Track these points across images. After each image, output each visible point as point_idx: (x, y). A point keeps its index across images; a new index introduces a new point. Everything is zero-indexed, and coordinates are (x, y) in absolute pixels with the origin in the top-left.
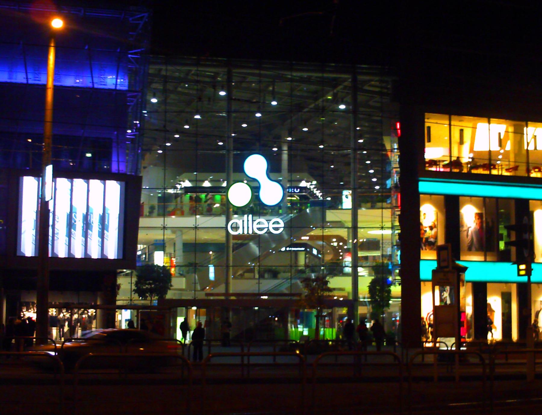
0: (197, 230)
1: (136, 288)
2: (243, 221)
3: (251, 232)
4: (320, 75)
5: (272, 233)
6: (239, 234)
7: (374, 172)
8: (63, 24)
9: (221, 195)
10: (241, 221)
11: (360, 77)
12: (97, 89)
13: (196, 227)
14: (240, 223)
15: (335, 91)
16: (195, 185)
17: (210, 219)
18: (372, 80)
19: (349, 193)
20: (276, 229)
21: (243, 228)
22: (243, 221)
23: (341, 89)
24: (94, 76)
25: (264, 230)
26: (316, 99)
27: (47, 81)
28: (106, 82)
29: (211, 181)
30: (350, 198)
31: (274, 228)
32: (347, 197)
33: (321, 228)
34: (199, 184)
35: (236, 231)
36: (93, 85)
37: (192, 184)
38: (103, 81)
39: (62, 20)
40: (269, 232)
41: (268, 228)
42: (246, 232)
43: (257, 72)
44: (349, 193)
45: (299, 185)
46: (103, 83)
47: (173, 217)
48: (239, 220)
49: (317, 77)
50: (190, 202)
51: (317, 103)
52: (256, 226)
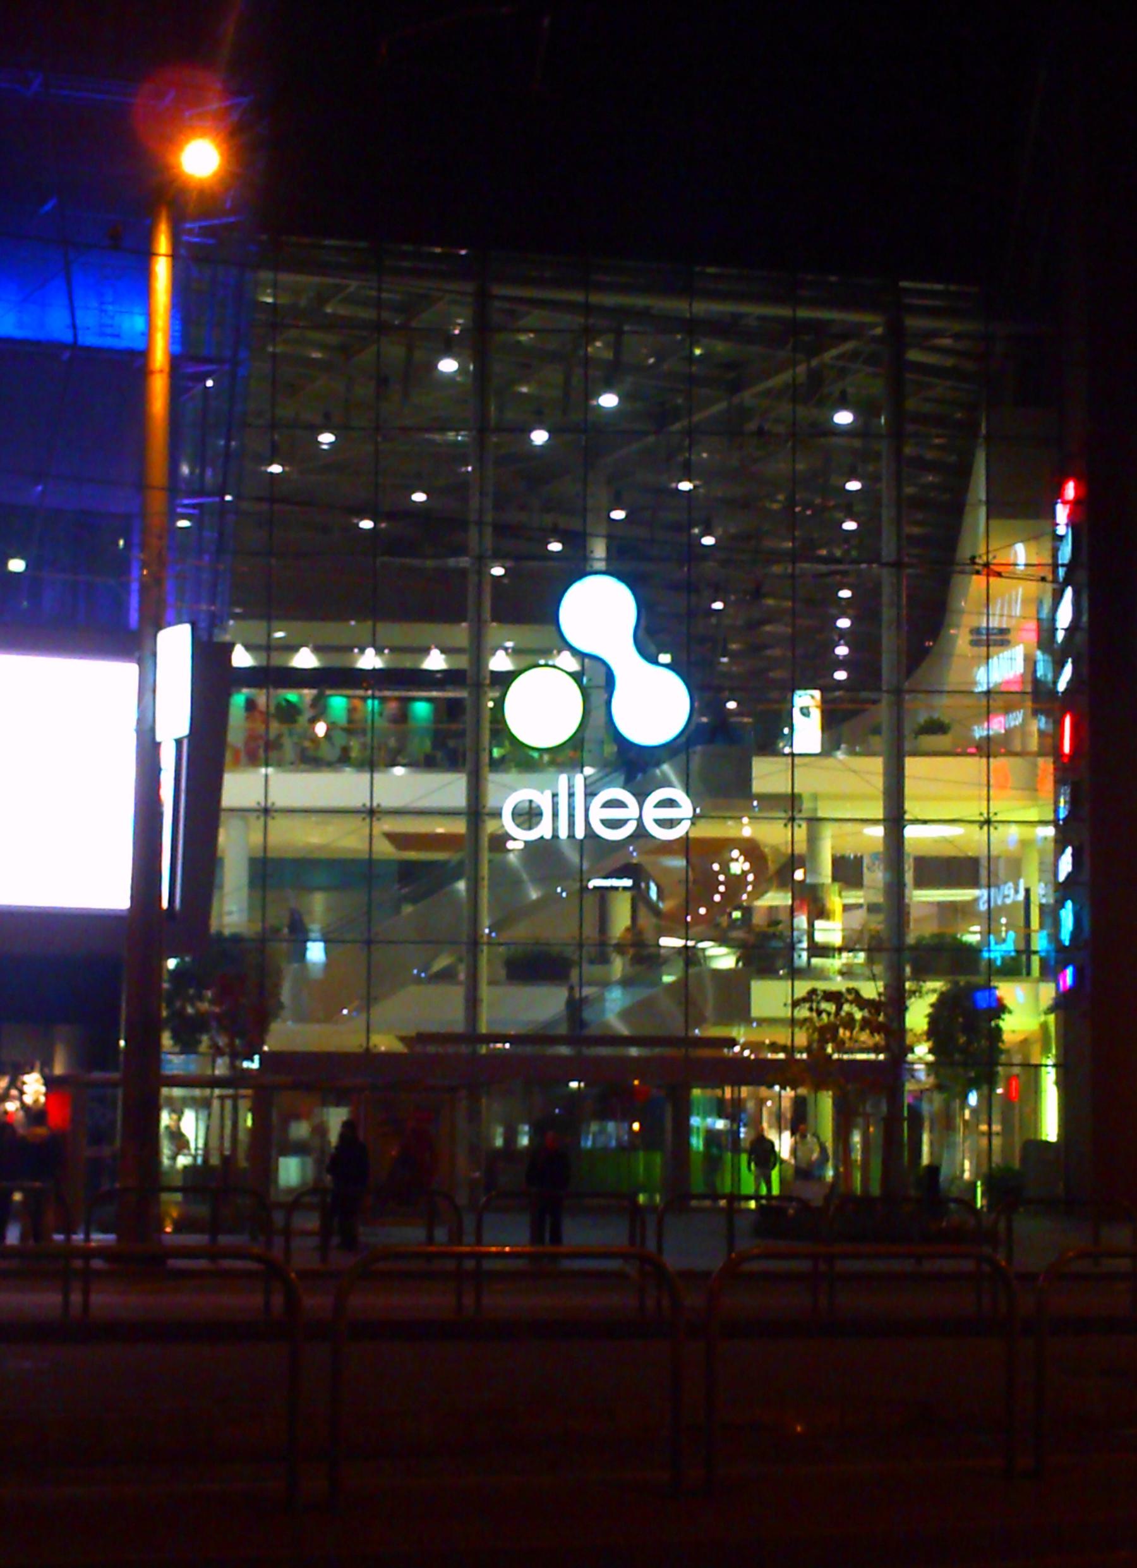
0: (374, 819)
1: (868, 1031)
2: (555, 795)
3: (580, 834)
4: (784, 312)
5: (598, 837)
6: (542, 838)
7: (835, 623)
8: (220, 166)
9: (348, 697)
10: (548, 794)
11: (913, 323)
12: (88, 348)
13: (988, 822)
14: (543, 801)
15: (814, 363)
16: (264, 663)
17: (449, 783)
18: (935, 334)
19: (813, 697)
20: (670, 824)
21: (555, 815)
22: (555, 795)
23: (832, 358)
24: (76, 304)
25: (679, 827)
26: (736, 387)
27: (148, 334)
28: (120, 327)
29: (317, 649)
30: (816, 714)
31: (659, 822)
32: (805, 712)
33: (363, 815)
34: (277, 660)
35: (530, 828)
36: (75, 336)
37: (255, 658)
38: (109, 322)
39: (222, 155)
40: (641, 833)
41: (640, 820)
42: (563, 834)
43: (576, 296)
44: (813, 697)
45: (422, 662)
46: (109, 331)
47: (399, 771)
48: (542, 793)
49: (763, 318)
50: (247, 718)
51: (736, 400)
52: (598, 813)
